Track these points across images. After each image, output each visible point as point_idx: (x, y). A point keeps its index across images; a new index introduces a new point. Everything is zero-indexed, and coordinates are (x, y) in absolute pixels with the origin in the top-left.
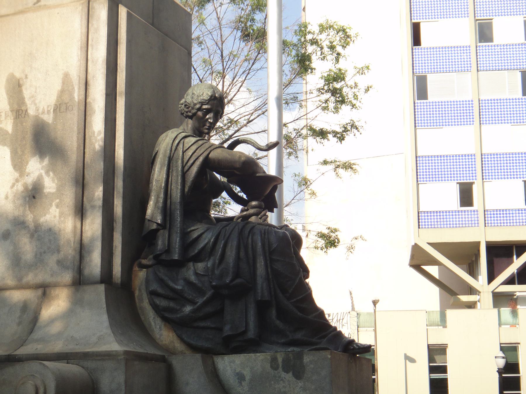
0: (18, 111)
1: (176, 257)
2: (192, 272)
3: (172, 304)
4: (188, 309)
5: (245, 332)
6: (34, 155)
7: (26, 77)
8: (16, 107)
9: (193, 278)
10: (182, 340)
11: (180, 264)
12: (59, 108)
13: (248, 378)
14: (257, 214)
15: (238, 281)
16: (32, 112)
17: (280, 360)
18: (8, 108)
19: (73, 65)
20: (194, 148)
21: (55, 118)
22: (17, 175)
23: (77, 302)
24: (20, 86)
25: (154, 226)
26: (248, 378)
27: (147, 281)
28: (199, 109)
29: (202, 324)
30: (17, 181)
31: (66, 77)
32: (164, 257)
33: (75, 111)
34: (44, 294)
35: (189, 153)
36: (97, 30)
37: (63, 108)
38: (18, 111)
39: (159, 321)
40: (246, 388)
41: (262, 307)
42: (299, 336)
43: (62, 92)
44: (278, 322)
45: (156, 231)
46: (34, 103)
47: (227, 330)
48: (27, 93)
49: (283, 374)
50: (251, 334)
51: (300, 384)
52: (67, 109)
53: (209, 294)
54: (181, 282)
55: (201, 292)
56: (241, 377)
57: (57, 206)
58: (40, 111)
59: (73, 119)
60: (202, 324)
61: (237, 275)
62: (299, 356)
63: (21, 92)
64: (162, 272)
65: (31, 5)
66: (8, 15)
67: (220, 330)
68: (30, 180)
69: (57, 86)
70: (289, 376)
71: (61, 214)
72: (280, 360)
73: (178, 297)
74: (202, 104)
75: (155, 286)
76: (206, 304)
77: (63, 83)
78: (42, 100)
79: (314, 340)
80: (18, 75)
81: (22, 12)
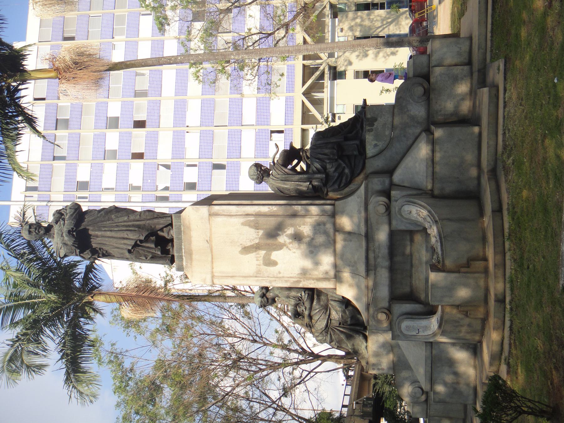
0: (256, 248)
1: (324, 176)
2: (331, 168)
3: (344, 178)
4: (347, 171)
5: (357, 145)
6: (276, 239)
7: (241, 244)
8: (254, 249)
9: (333, 169)
10: (359, 174)
11: (327, 175)
12: (256, 227)
13: (376, 142)
14: (306, 152)
15: (335, 147)
16: (257, 241)
17: (369, 128)
18: (254, 253)
19: (238, 221)
20: (277, 171)
21: (261, 229)
22: (285, 248)
23: (343, 213)
24: (245, 248)
25: (311, 186)
26: (376, 142)
27: (334, 191)
28: (260, 172)
29: (353, 164)
30: (287, 247)
31: (244, 224)
32: (324, 182)
33: (259, 219)
34: (338, 231)
35: (279, 172)
36: (223, 211)
37: (257, 225)
38: (256, 248)
39: (350, 186)
40: (380, 143)
41: (346, 139)
42: (359, 126)
43: (250, 226)
44: (353, 133)
45: (312, 185)
46: (253, 240)
47: (356, 153)
48: (249, 244)
49: (375, 126)
50: (357, 142)
51: (379, 119)
52: (257, 223)
53: (340, 161)
54: (335, 174)
55: (339, 165)
56: (376, 145)
57: (300, 227)
58: (257, 236)
59: (261, 220)
60: (353, 164)
61: (334, 148)
62: (368, 119)
63: (248, 247)
64: (330, 183)
65: (208, 245)
66: (212, 255)
67: (356, 156)
68: (288, 241)
69: (247, 228)
70: (376, 124)
71: (304, 224)
72: (369, 128)
73: (341, 175)
74: (258, 170)
75: (336, 186)
76: (345, 163)
77: (246, 225)
78: (252, 236)
79: (360, 120)
80: (240, 249)
81: (211, 250)
